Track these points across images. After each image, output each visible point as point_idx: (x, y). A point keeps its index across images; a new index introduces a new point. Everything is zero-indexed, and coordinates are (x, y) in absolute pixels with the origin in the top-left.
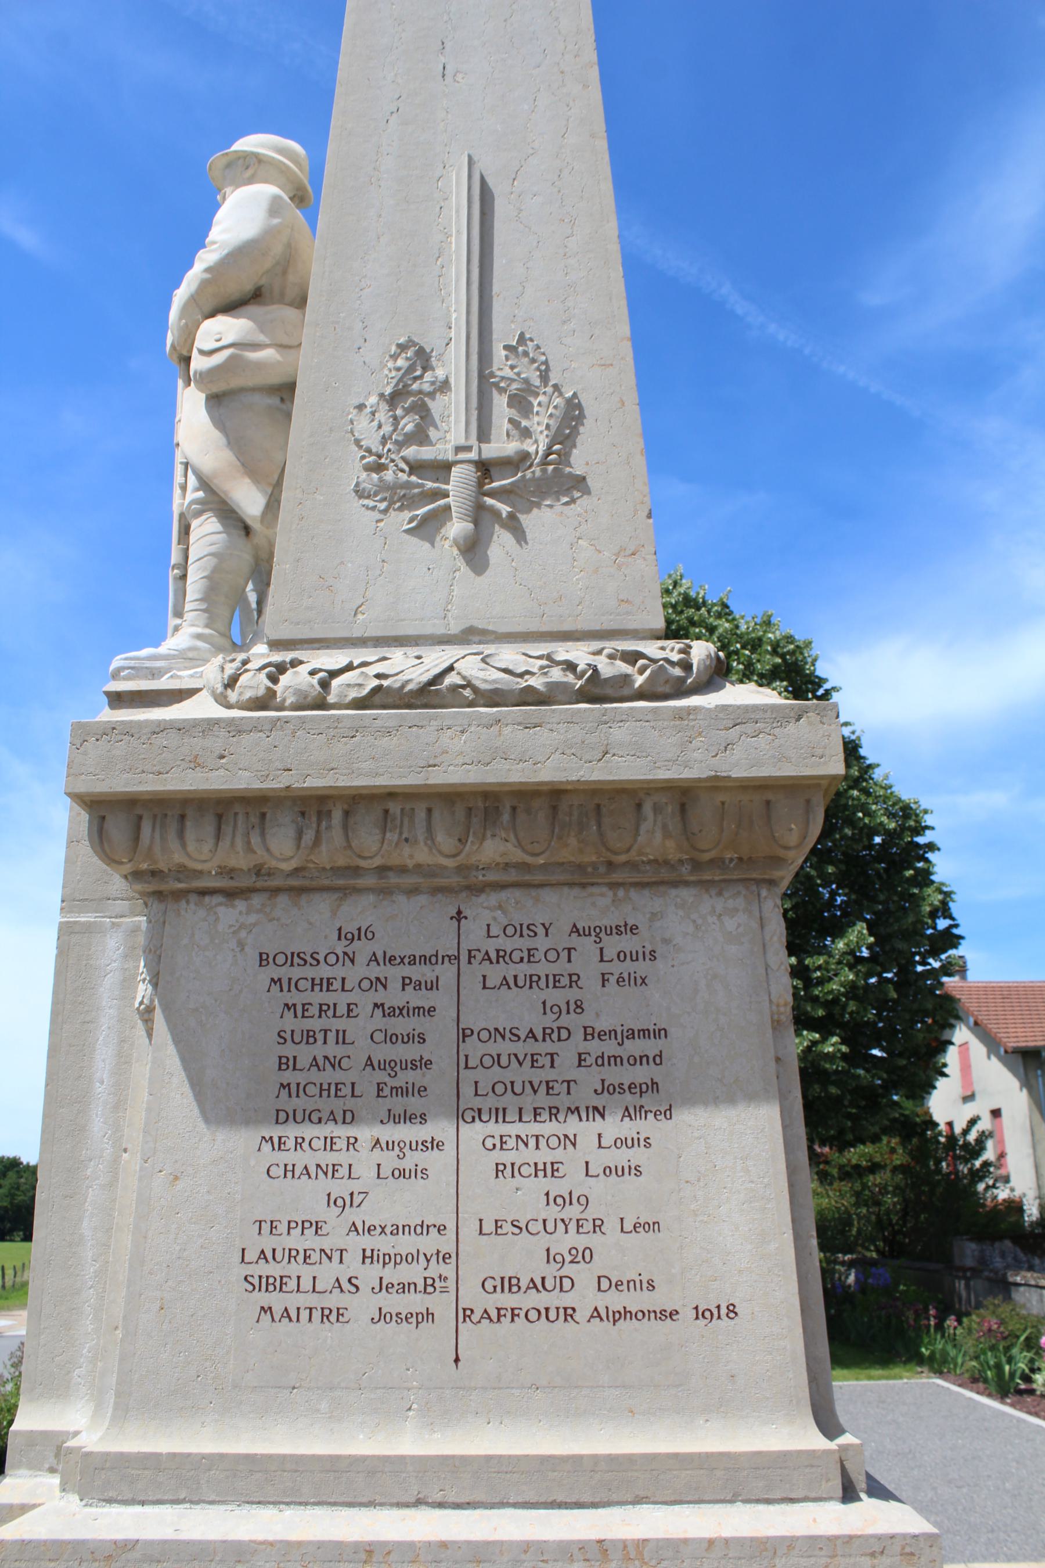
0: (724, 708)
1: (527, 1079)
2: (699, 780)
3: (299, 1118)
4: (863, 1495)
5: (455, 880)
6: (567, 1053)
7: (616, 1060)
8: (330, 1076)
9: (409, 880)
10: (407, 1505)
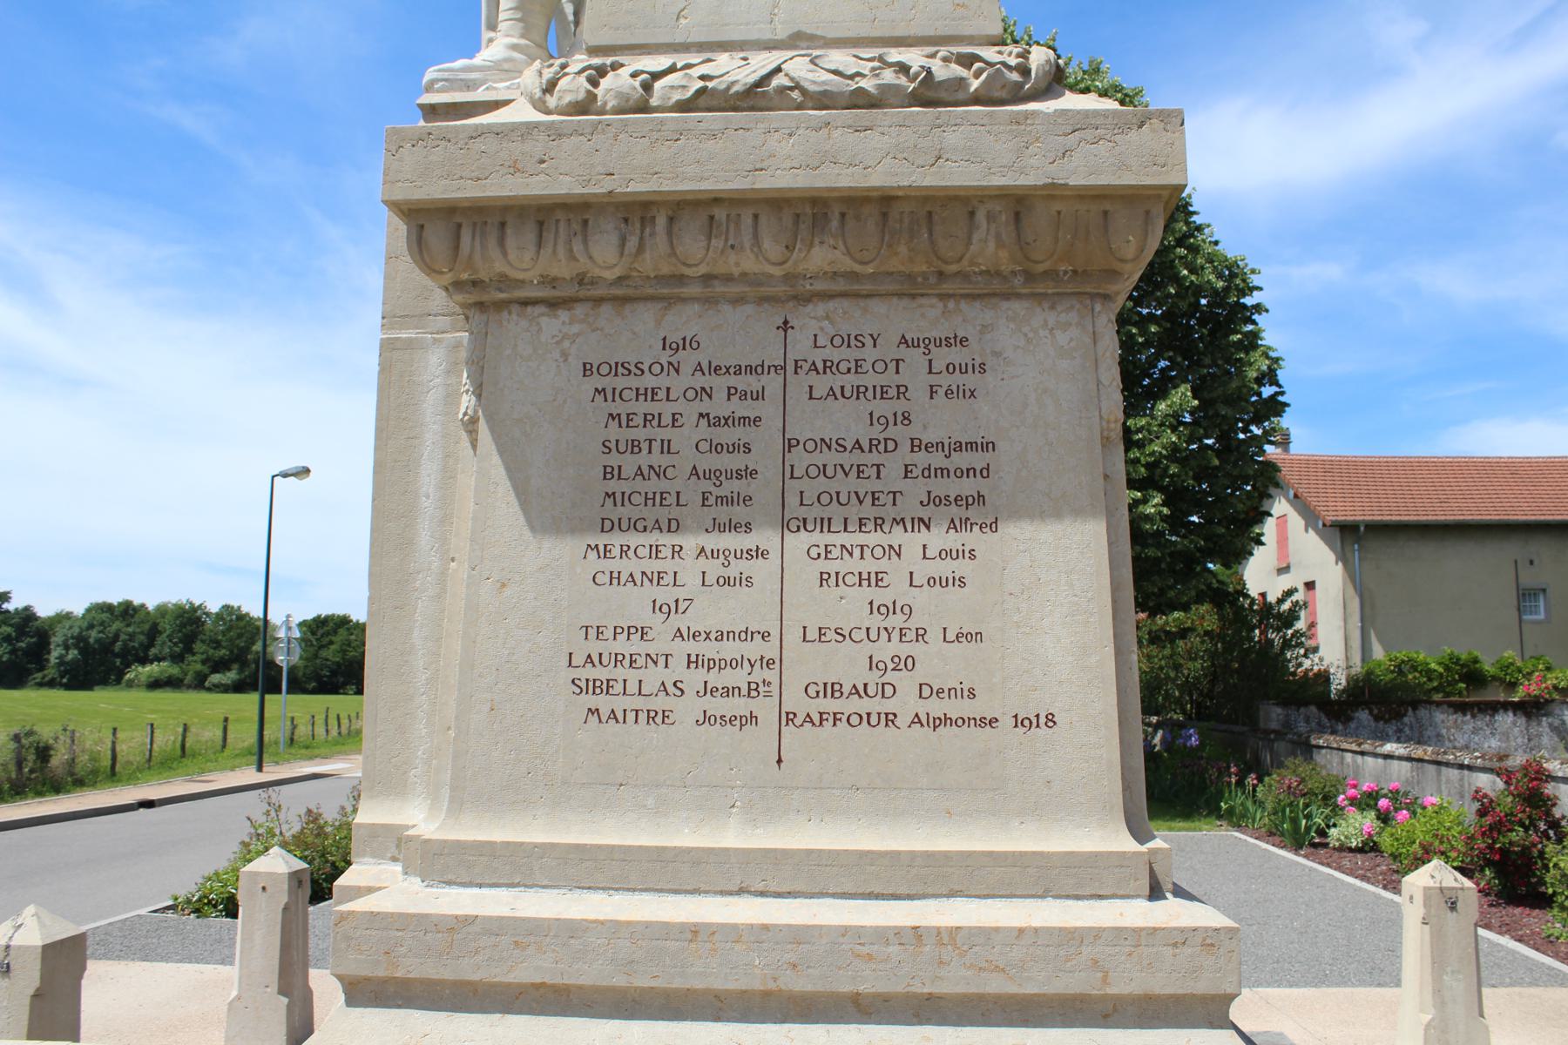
0: (1064, 112)
1: (853, 489)
2: (1035, 187)
3: (624, 527)
4: (1168, 895)
5: (780, 289)
6: (893, 465)
7: (943, 472)
8: (654, 485)
9: (735, 289)
10: (730, 893)
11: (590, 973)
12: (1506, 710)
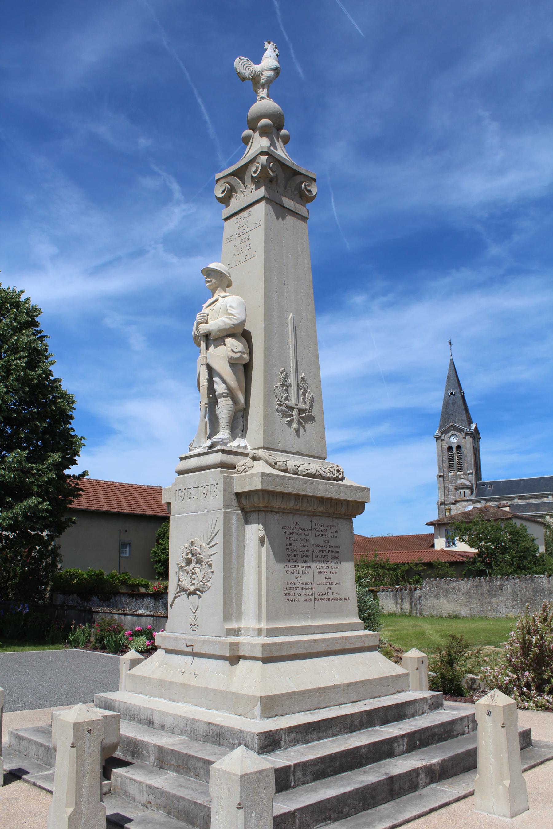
11: (301, 651)
12: (148, 597)
